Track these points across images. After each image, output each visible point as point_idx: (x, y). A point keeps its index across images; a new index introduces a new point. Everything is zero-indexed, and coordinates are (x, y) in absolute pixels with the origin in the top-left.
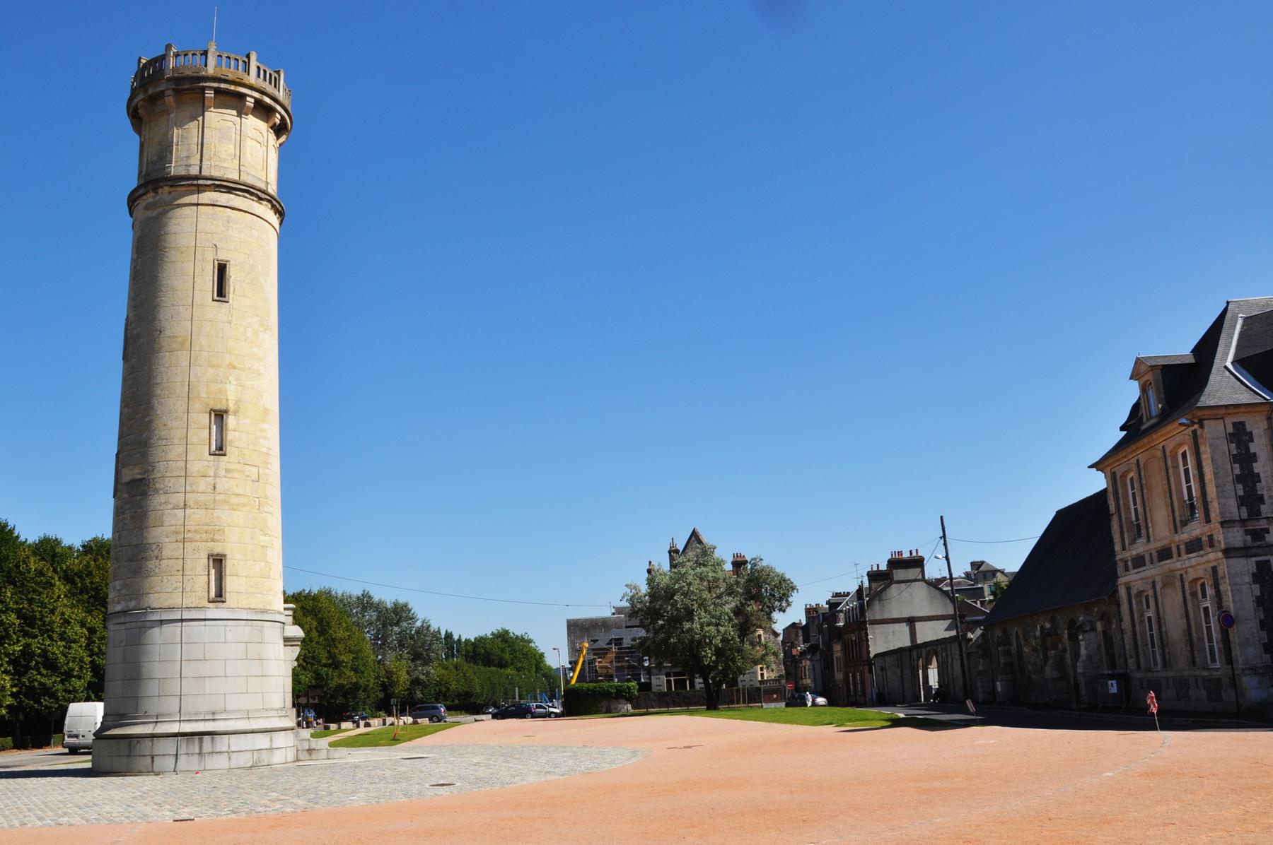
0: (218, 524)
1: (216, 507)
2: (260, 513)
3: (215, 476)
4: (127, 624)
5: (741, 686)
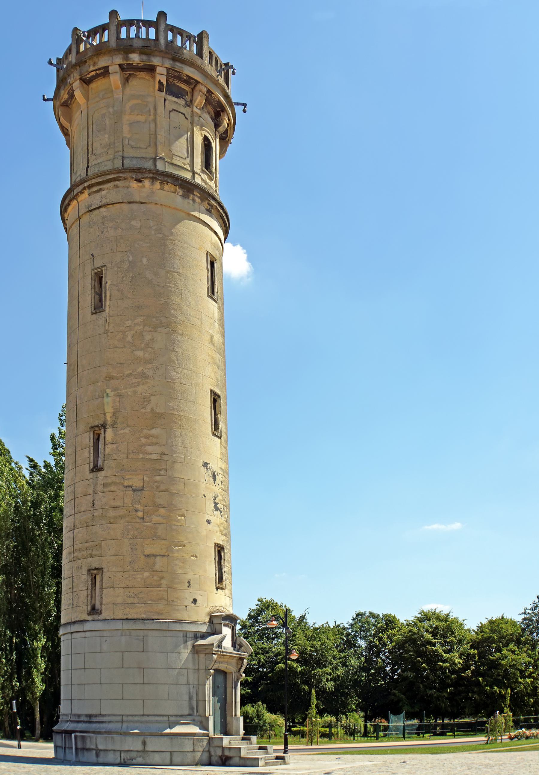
0: (95, 540)
1: (94, 523)
2: (145, 522)
3: (94, 492)
4: (87, 633)
5: (393, 732)
